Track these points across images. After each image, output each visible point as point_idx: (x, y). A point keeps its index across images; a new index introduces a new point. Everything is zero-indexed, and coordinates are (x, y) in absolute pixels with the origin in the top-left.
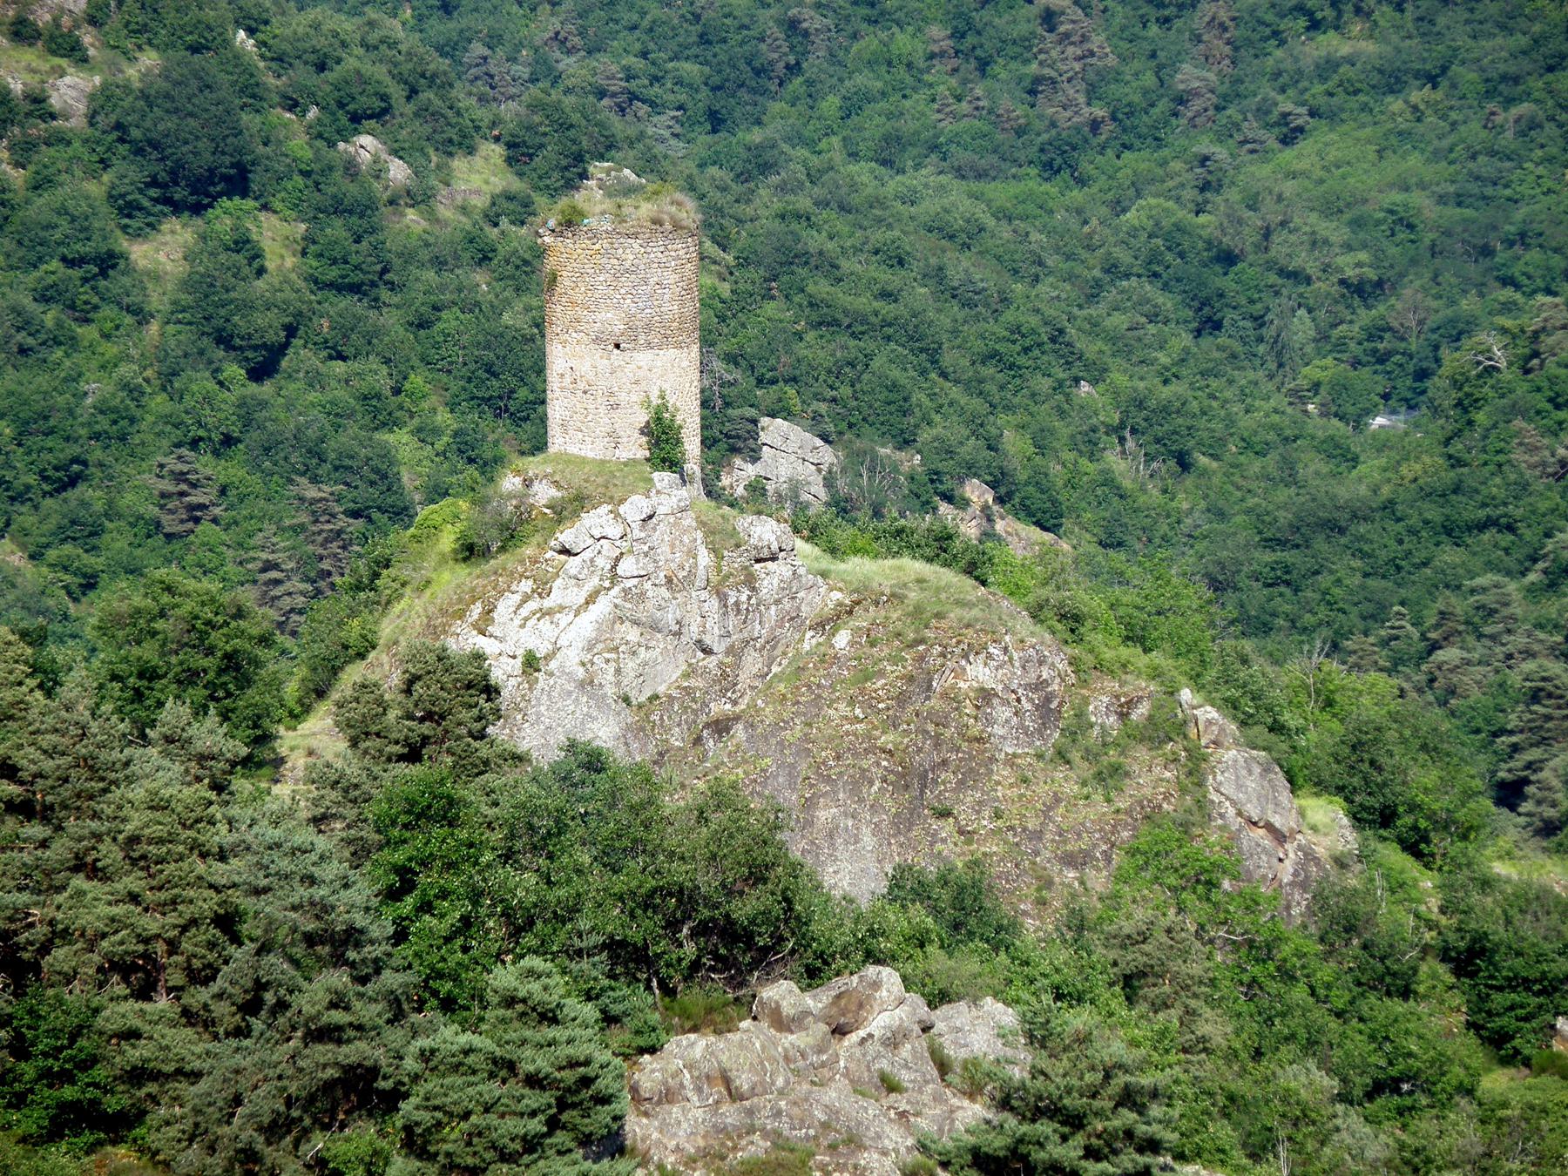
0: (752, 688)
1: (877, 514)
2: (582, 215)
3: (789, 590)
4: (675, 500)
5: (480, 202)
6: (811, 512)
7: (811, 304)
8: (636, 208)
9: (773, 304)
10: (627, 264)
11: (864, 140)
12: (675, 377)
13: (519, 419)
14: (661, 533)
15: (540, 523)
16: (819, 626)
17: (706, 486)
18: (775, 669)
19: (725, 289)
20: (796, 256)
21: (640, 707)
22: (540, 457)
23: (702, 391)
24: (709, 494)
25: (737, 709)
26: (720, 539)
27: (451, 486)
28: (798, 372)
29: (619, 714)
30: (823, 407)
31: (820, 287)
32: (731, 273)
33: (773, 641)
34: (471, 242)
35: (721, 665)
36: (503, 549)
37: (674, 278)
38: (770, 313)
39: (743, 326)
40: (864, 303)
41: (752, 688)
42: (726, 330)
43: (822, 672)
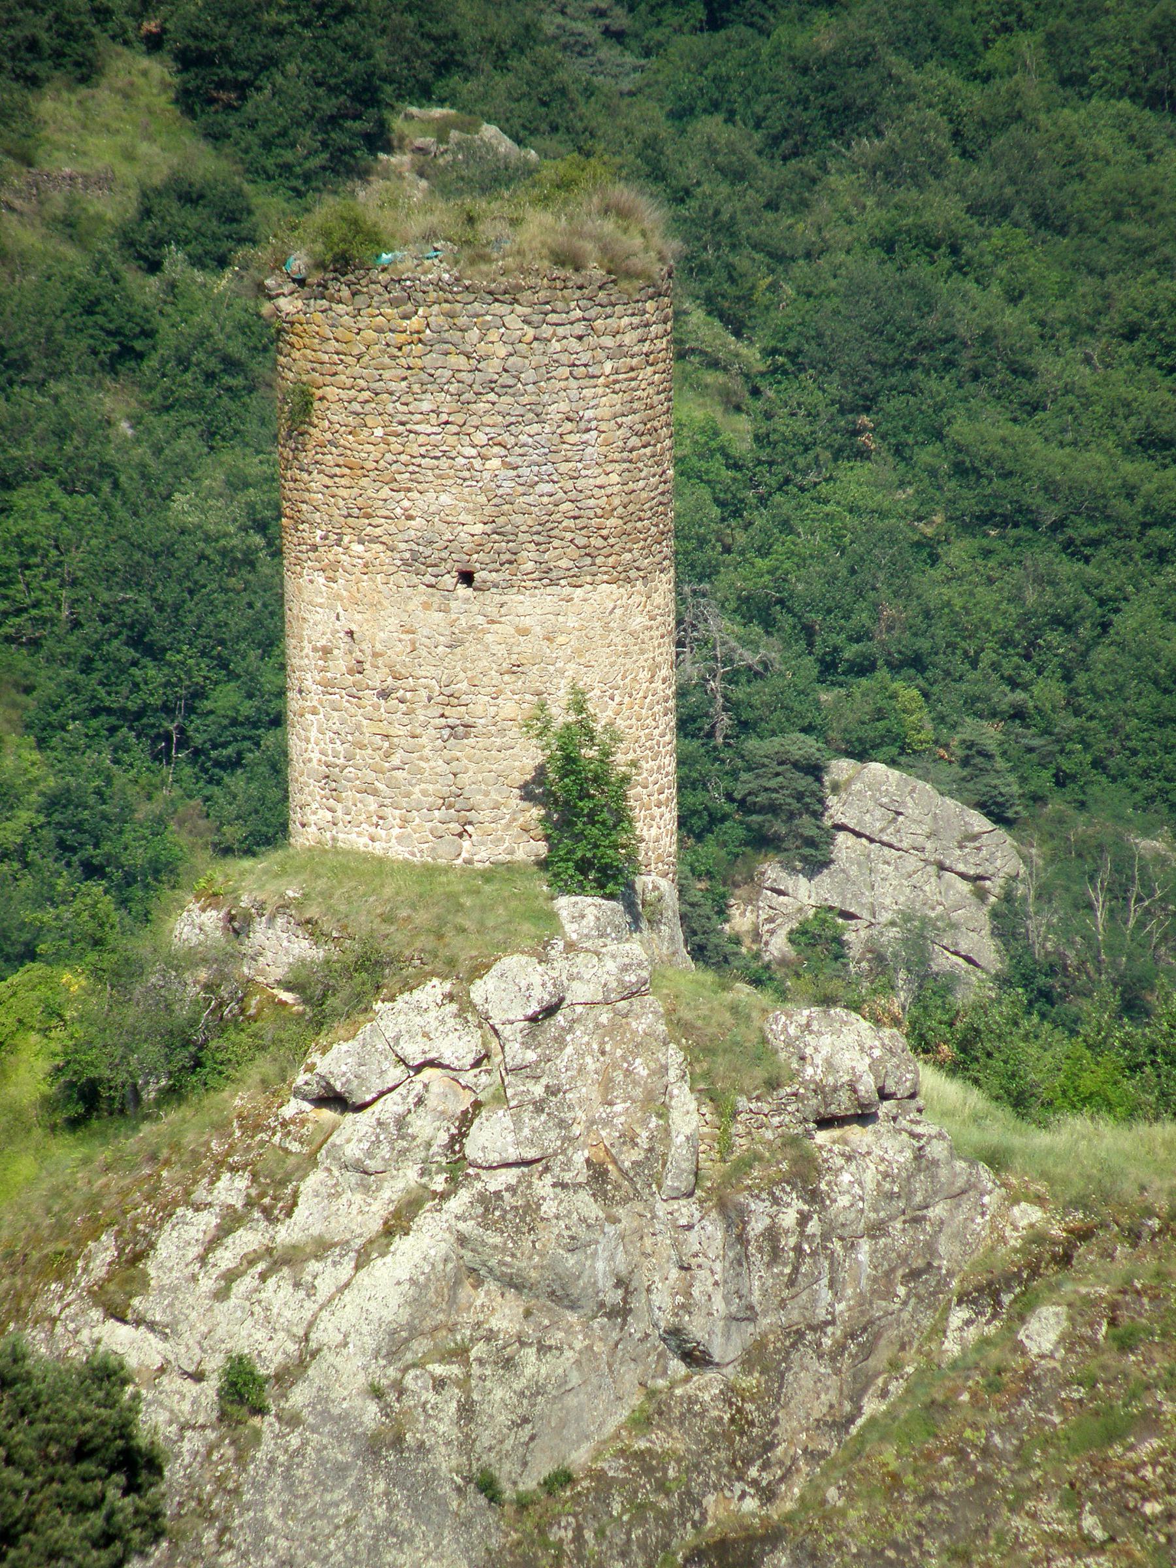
0: (813, 1456)
1: (1132, 1006)
2: (376, 240)
3: (904, 1198)
4: (611, 965)
5: (111, 208)
6: (962, 998)
7: (960, 470)
8: (515, 222)
9: (863, 470)
10: (492, 368)
11: (1103, 41)
12: (609, 653)
13: (214, 764)
14: (578, 1052)
15: (267, 1027)
16: (985, 1294)
17: (690, 933)
18: (872, 1406)
19: (739, 432)
20: (923, 346)
21: (523, 1504)
22: (270, 860)
23: (682, 693)
24: (699, 952)
25: (775, 1512)
26: (727, 1067)
27: (40, 931)
28: (924, 644)
29: (467, 1524)
30: (990, 734)
31: (983, 426)
32: (756, 392)
33: (864, 1333)
34: (89, 311)
35: (730, 1393)
36: (174, 1094)
37: (609, 403)
38: (854, 491)
39: (786, 526)
40: (1097, 465)
41: (813, 1456)
42: (741, 538)
43: (994, 1415)
